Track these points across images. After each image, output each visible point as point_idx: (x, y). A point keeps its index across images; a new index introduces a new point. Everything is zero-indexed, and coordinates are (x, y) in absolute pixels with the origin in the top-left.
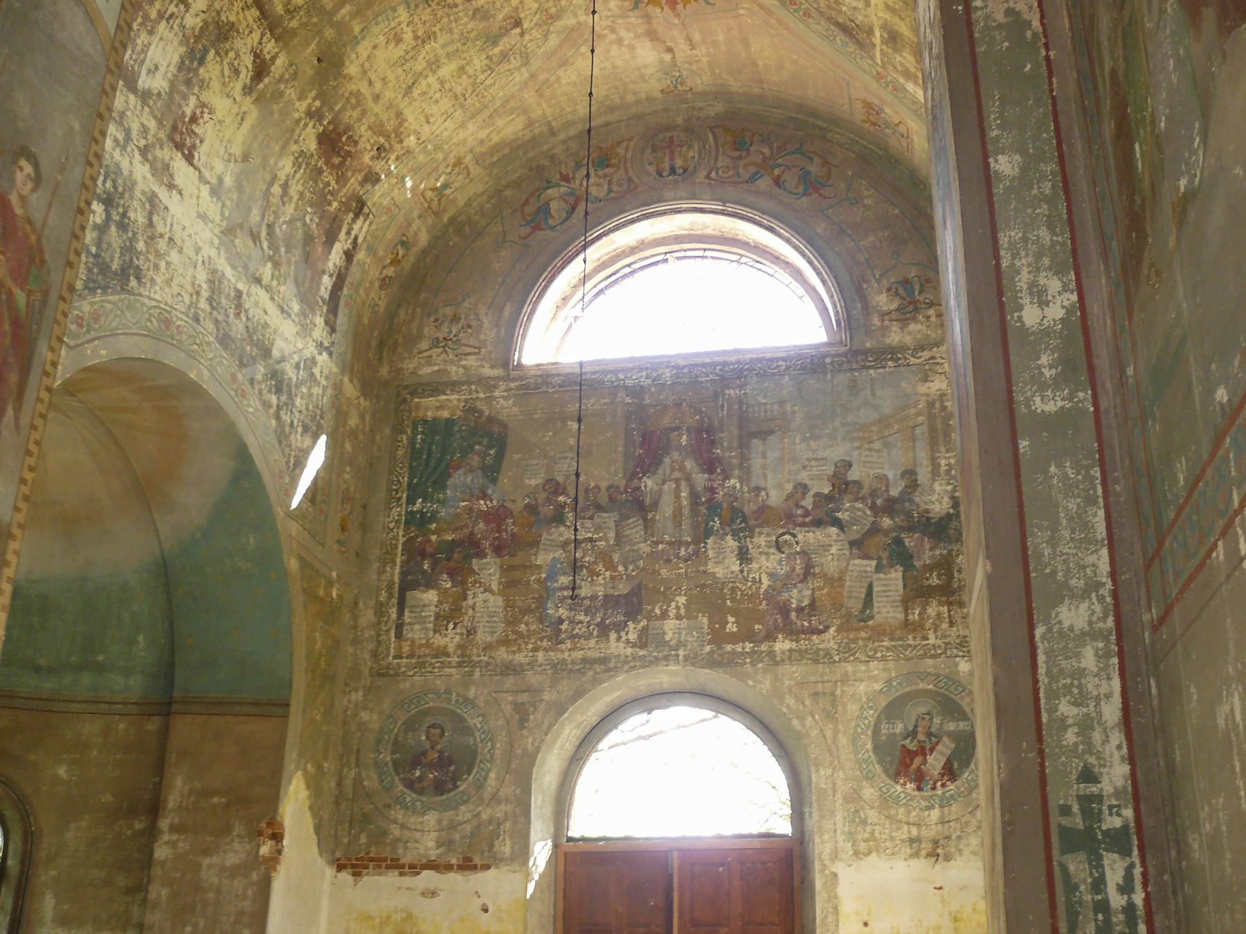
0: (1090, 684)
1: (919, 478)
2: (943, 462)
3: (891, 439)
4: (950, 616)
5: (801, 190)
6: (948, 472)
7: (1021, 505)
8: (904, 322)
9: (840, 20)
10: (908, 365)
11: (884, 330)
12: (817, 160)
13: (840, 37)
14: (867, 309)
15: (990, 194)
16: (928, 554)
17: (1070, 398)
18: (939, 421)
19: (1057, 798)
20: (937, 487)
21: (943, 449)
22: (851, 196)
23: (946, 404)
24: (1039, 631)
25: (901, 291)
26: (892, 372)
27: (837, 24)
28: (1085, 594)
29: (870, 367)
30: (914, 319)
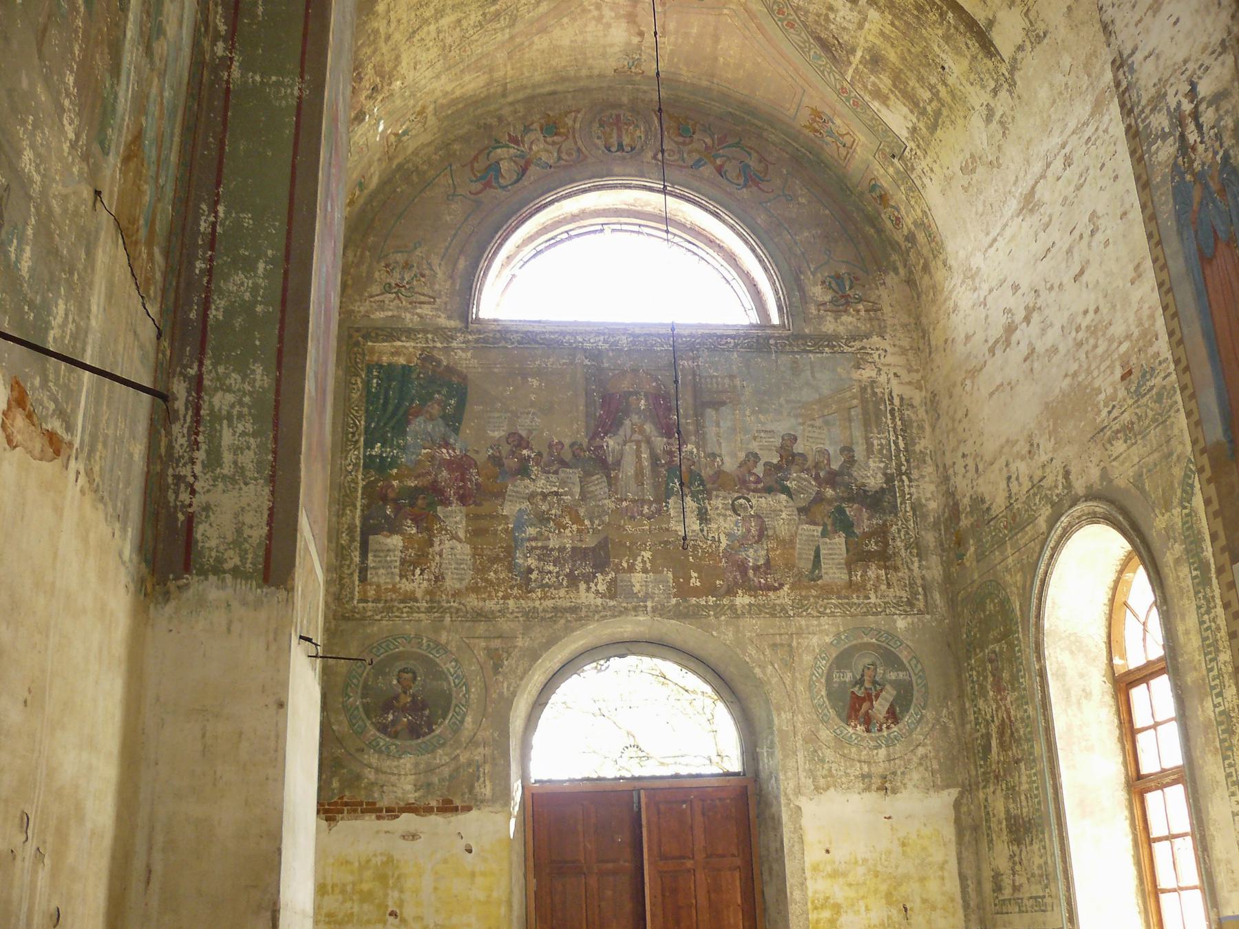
2: (875, 442)
3: (830, 417)
5: (742, 181)
6: (880, 451)
8: (837, 314)
9: (823, 35)
10: (842, 352)
11: (821, 318)
12: (754, 155)
14: (804, 298)
16: (866, 522)
18: (871, 406)
21: (875, 430)
23: (876, 390)
25: (834, 285)
27: (819, 39)
29: (810, 351)
30: (846, 311)
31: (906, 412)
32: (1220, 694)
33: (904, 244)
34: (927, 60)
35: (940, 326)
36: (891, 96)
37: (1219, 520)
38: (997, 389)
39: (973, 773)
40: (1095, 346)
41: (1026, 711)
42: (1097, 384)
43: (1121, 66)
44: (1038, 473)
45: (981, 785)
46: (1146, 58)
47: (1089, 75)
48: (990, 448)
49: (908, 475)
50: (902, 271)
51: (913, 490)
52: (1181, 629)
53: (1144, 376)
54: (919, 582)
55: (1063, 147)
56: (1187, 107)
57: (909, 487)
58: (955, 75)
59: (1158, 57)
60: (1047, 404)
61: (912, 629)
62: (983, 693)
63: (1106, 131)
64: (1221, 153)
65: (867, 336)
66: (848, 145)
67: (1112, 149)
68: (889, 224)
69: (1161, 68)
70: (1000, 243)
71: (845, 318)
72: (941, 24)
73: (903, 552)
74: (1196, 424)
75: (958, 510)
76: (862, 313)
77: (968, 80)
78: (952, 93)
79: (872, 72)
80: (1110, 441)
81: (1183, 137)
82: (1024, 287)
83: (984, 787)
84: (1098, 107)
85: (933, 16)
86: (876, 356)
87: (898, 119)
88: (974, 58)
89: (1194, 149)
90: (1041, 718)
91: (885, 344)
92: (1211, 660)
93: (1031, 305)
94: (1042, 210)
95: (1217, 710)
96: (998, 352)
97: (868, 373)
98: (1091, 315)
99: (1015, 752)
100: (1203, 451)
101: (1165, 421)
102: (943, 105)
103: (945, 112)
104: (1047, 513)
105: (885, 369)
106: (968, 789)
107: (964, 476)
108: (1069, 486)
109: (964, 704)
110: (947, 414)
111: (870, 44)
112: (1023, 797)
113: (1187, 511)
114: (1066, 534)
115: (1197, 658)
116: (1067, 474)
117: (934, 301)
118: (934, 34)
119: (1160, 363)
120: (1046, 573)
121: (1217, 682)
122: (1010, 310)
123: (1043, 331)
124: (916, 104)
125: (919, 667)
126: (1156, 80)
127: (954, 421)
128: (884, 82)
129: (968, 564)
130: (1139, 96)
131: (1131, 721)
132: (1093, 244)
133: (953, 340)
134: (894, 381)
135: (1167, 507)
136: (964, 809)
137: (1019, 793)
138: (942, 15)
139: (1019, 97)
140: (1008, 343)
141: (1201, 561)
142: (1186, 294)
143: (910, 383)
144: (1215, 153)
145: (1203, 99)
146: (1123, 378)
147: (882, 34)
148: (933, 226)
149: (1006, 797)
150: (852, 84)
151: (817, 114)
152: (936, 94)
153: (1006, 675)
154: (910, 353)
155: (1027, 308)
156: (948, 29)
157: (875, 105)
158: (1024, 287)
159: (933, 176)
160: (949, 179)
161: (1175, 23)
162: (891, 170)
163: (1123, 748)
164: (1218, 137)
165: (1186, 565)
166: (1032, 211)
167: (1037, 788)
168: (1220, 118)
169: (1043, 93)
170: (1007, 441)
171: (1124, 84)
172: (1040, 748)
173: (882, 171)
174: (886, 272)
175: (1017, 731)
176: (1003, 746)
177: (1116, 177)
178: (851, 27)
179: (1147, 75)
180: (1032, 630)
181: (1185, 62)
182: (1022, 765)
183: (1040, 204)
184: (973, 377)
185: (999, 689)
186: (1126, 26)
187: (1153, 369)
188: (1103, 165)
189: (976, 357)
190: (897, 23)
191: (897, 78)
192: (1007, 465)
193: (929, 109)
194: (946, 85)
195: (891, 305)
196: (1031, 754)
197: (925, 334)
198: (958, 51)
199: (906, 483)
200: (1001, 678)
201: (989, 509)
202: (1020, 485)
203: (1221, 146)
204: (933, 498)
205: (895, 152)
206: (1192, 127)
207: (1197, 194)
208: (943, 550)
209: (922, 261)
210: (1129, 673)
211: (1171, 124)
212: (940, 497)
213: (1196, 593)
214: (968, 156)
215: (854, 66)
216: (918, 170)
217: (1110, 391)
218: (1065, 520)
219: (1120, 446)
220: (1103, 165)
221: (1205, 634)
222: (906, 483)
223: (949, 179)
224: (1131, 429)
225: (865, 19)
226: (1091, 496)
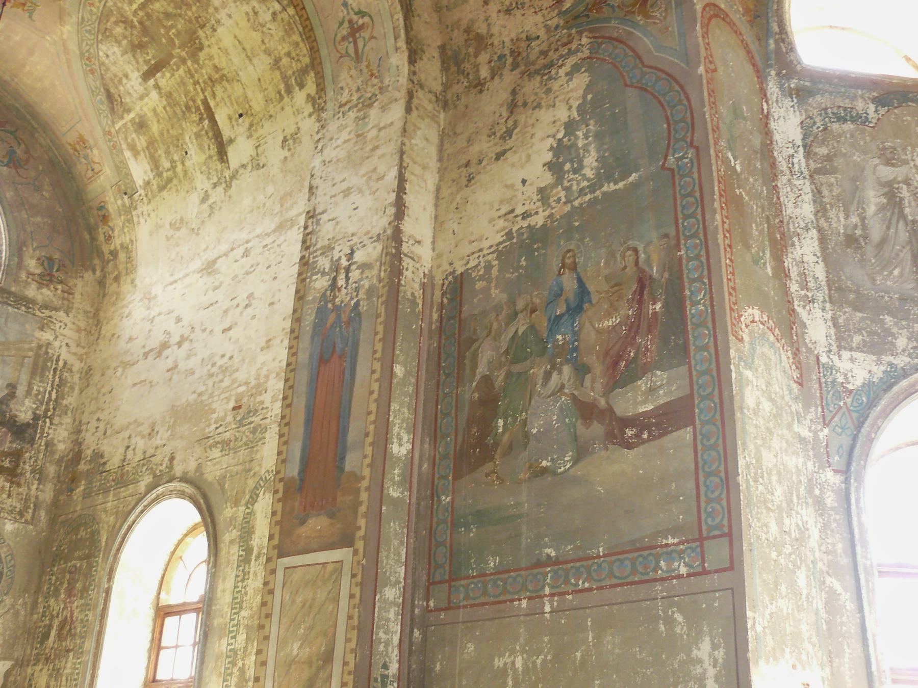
0: (391, 625)
1: (18, 392)
2: (35, 388)
3: (8, 359)
4: (9, 491)
5: (5, 161)
6: (37, 395)
7: (379, 538)
8: (41, 285)
9: (112, 90)
10: (34, 314)
11: (27, 284)
12: (23, 146)
13: (102, 97)
14: (20, 265)
15: (391, 383)
16: (8, 445)
17: (402, 493)
18: (41, 360)
19: (374, 675)
20: (27, 402)
21: (38, 379)
22: (37, 184)
23: (49, 350)
24: (377, 597)
25: (46, 264)
26: (22, 315)
27: (108, 92)
28: (394, 586)
29: (10, 305)
30: (47, 286)
31: (66, 374)
32: (234, 637)
33: (107, 256)
34: (177, 142)
35: (112, 323)
36: (142, 153)
37: (278, 527)
38: (140, 383)
39: (28, 652)
40: (222, 381)
41: (87, 615)
42: (214, 406)
43: (312, 217)
44: (150, 452)
45: (32, 663)
46: (329, 220)
47: (282, 206)
48: (120, 421)
49: (51, 419)
50: (98, 273)
51: (51, 431)
52: (220, 587)
53: (249, 412)
54: (33, 499)
55: (247, 242)
56: (344, 263)
57: (49, 428)
58: (192, 162)
59: (337, 223)
60: (173, 406)
61: (16, 534)
62: (56, 594)
63: (279, 246)
64: (355, 300)
65: (56, 309)
66: (96, 170)
67: (279, 258)
68: (101, 238)
69: (337, 230)
70: (179, 285)
71: (45, 290)
72: (198, 125)
73: (28, 474)
74: (283, 460)
75: (80, 456)
76: (59, 292)
77: (200, 169)
78: (185, 172)
79: (136, 131)
80: (210, 447)
81: (335, 280)
82: (185, 322)
83: (35, 665)
84: (280, 228)
85: (195, 117)
86: (58, 326)
87: (139, 170)
88: (210, 157)
89: (339, 290)
90: (97, 623)
91: (67, 320)
92: (235, 614)
93: (186, 336)
94: (217, 276)
95: (229, 647)
96: (150, 357)
97: (47, 336)
98: (226, 359)
99: (68, 643)
100: (281, 480)
101: (253, 447)
102: (175, 176)
103: (175, 181)
104: (149, 481)
105: (61, 338)
106: (21, 664)
107: (93, 434)
108: (171, 467)
109: (38, 598)
110: (96, 385)
111: (142, 113)
112: (64, 678)
113: (248, 511)
114: (157, 499)
115: (226, 609)
116: (172, 459)
117: (114, 304)
118: (190, 129)
119: (263, 409)
120: (134, 522)
121: (235, 628)
122: (169, 333)
123: (188, 357)
124: (157, 168)
125: (12, 562)
126: (331, 237)
127: (99, 392)
128: (141, 142)
129: (75, 497)
130: (317, 241)
131: (160, 640)
132: (245, 314)
133: (119, 337)
134: (64, 349)
135: (236, 503)
136: (12, 678)
137: (61, 675)
138: (201, 120)
139: (230, 197)
140: (159, 354)
141: (248, 546)
142: (303, 377)
143: (75, 354)
144: (352, 299)
145: (355, 263)
146: (234, 409)
147: (154, 110)
148: (134, 252)
149: (50, 676)
150: (118, 132)
151: (82, 140)
152: (173, 168)
153: (79, 586)
154: (83, 333)
155: (182, 336)
156: (201, 130)
157: (128, 154)
158: (185, 322)
159: (148, 219)
160: (158, 227)
161: (355, 209)
162: (119, 202)
163: (149, 658)
164: (357, 290)
165: (237, 546)
166: (209, 274)
167: (78, 674)
168: (362, 279)
169: (247, 202)
170: (136, 421)
171: (310, 229)
172: (89, 645)
173: (112, 200)
174: (87, 270)
175: (75, 628)
176: (59, 637)
177: (275, 278)
178: (135, 95)
179: (326, 231)
180: (111, 559)
181: (353, 235)
182: (71, 654)
183: (216, 272)
184: (124, 368)
185: (70, 593)
186: (325, 194)
187: (256, 411)
188: (269, 266)
189: (132, 355)
190: (168, 109)
191: (151, 143)
192: (129, 437)
193: (165, 174)
194: (183, 164)
195: (82, 294)
196: (81, 648)
197: (98, 324)
198: (201, 147)
199: (48, 424)
200: (73, 588)
201: (105, 463)
202: (135, 454)
203: (357, 296)
204: (64, 441)
205: (128, 192)
206: (342, 276)
207: (332, 318)
208: (59, 481)
209: (116, 273)
210: (169, 606)
211: (331, 268)
212: (69, 442)
213: (238, 566)
214: (179, 218)
215: (124, 121)
216: (140, 210)
217: (222, 414)
218: (160, 489)
219: (216, 453)
220: (269, 266)
221: (236, 595)
222: (48, 424)
223: (158, 227)
224: (228, 445)
225: (147, 95)
226: (184, 479)
